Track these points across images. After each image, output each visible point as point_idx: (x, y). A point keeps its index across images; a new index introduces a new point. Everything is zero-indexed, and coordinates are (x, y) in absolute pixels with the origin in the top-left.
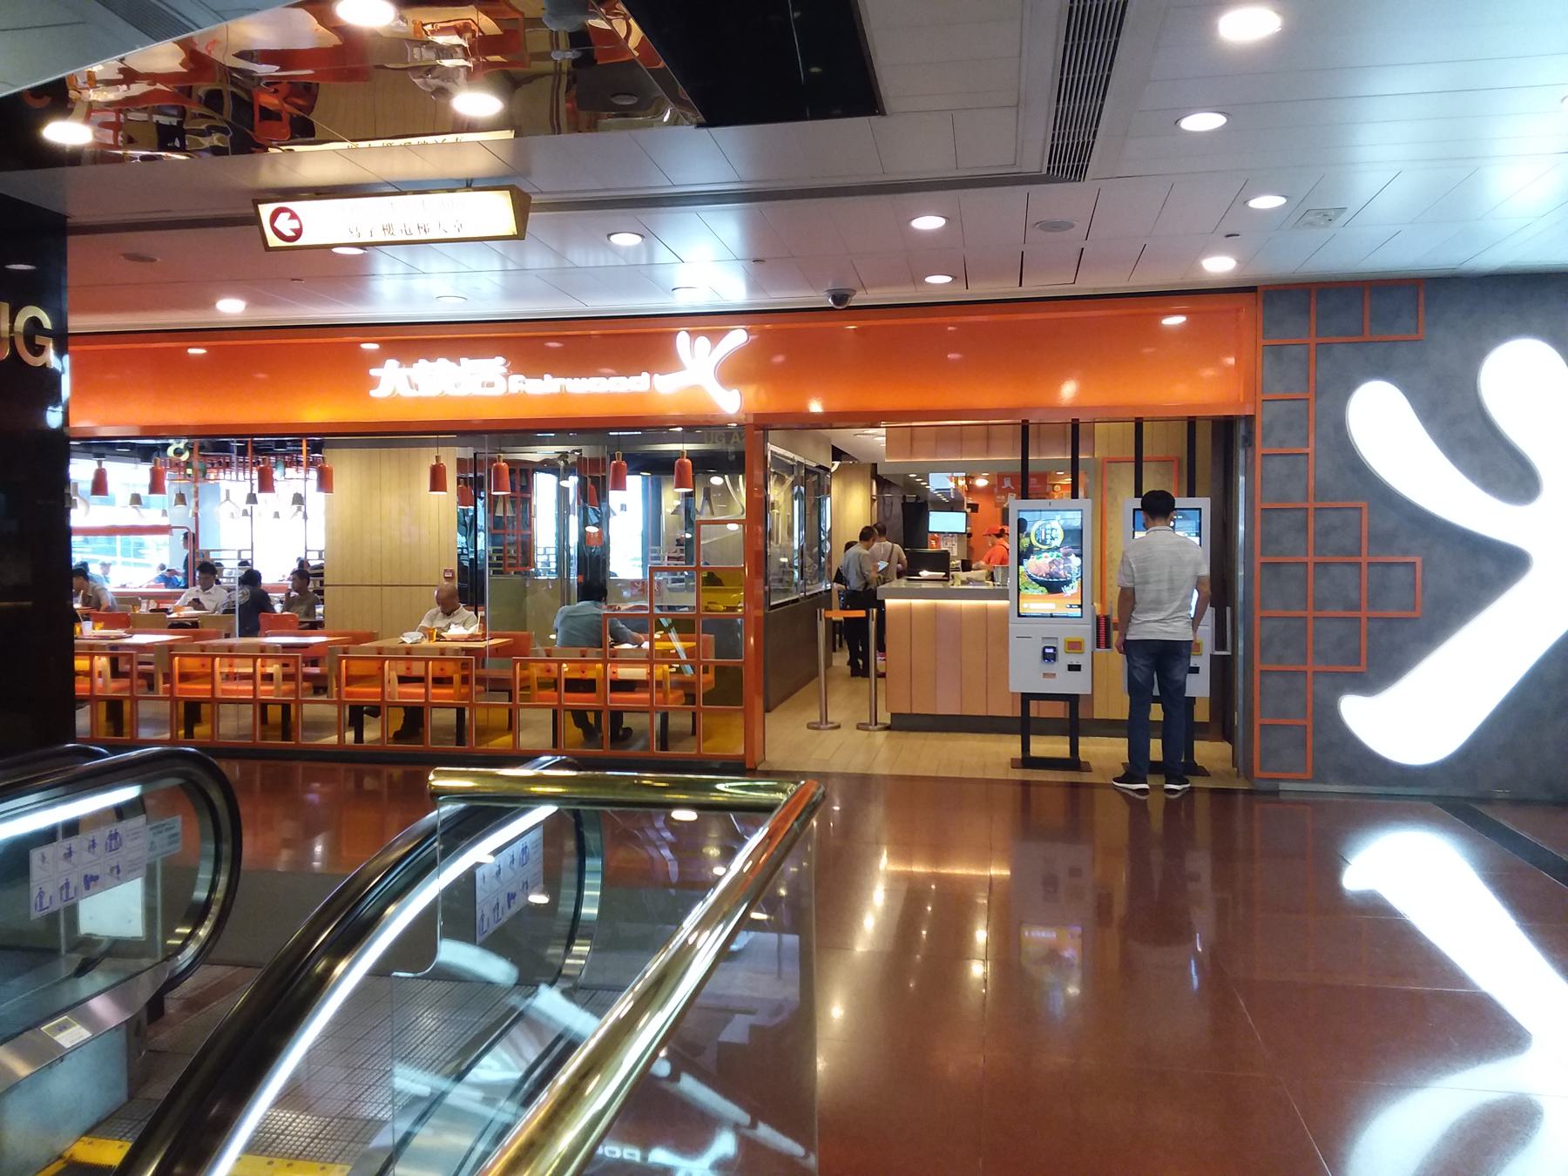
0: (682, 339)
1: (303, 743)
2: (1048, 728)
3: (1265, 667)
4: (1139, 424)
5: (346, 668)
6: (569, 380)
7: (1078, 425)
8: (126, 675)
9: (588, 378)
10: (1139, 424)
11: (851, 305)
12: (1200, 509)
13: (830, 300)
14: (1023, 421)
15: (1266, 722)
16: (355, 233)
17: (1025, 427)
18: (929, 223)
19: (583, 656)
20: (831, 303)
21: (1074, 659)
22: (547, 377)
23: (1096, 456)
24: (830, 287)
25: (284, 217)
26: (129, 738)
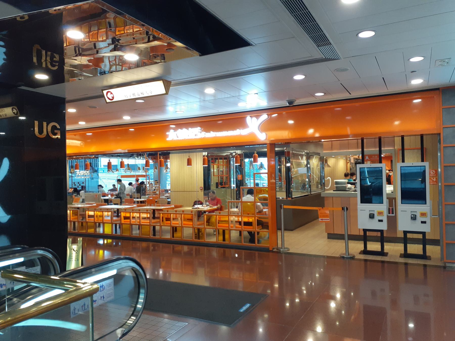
0: (248, 119)
1: (80, 232)
2: (374, 239)
3: (447, 222)
4: (422, 136)
5: (184, 216)
6: (217, 133)
7: (364, 140)
8: (159, 218)
9: (233, 131)
10: (403, 137)
11: (294, 105)
12: (401, 167)
13: (288, 104)
14: (361, 138)
15: (448, 242)
16: (126, 97)
17: (380, 139)
18: (299, 77)
19: (248, 215)
20: (288, 105)
21: (380, 218)
22: (211, 132)
23: (395, 148)
24: (287, 99)
25: (109, 93)
26: (77, 231)
